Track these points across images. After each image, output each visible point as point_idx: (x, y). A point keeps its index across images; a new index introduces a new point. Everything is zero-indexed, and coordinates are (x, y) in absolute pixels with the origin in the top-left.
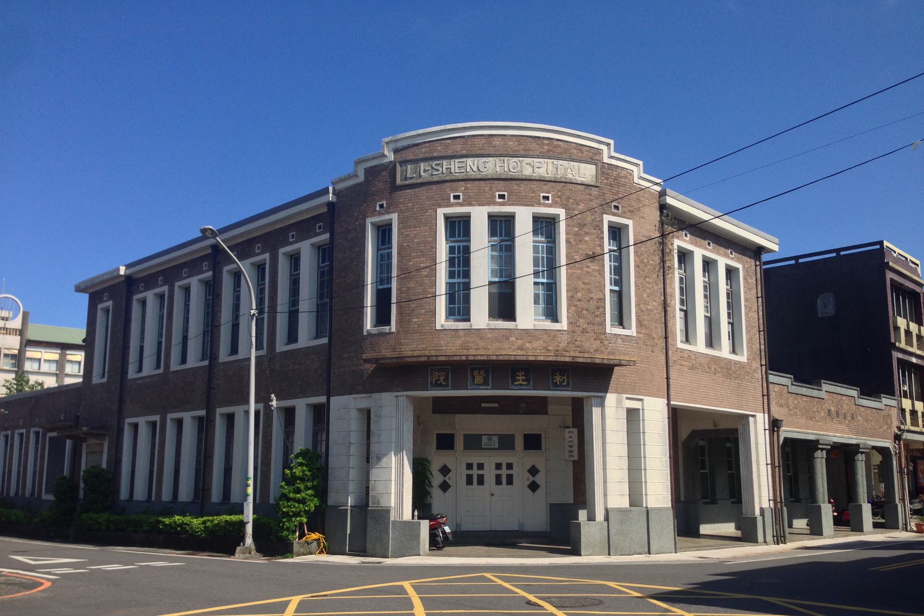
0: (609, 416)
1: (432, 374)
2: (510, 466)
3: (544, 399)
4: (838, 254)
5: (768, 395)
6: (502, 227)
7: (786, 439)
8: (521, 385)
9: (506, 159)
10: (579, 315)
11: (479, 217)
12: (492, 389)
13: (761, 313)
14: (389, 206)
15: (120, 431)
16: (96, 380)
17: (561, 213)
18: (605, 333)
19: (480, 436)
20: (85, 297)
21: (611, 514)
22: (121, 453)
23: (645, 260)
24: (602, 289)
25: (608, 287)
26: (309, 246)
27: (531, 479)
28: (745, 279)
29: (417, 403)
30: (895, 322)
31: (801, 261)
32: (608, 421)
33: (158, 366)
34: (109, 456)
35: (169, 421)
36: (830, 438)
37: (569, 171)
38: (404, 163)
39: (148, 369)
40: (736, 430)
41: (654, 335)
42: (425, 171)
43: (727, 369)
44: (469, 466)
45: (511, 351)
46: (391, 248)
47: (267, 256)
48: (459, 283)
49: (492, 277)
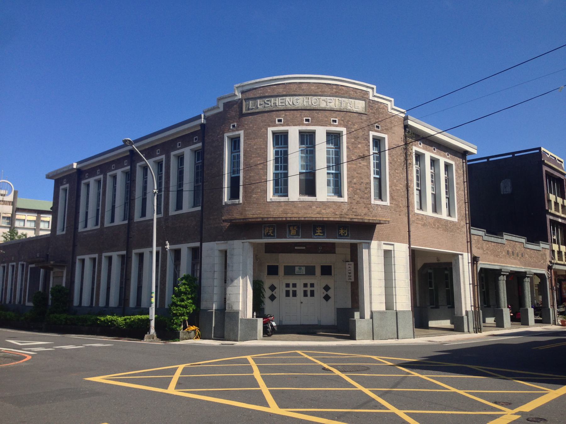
0: (373, 255)
1: (264, 229)
2: (312, 285)
3: (333, 244)
4: (513, 155)
5: (471, 242)
6: (308, 139)
7: (481, 269)
8: (319, 235)
9: (310, 97)
10: (355, 193)
11: (294, 133)
12: (301, 238)
13: (466, 192)
14: (238, 126)
15: (74, 263)
16: (59, 232)
17: (344, 130)
18: (371, 204)
19: (294, 267)
20: (52, 182)
21: (374, 315)
22: (74, 277)
23: (395, 159)
24: (369, 177)
25: (372, 176)
27: (325, 293)
28: (456, 171)
29: (256, 247)
30: (548, 197)
31: (490, 159)
32: (373, 258)
33: (97, 224)
34: (67, 279)
35: (103, 257)
36: (508, 268)
37: (349, 104)
38: (247, 99)
39: (91, 226)
40: (451, 263)
41: (401, 205)
43: (445, 226)
44: (288, 285)
45: (313, 215)
46: (239, 152)
47: (163, 157)
48: (281, 173)
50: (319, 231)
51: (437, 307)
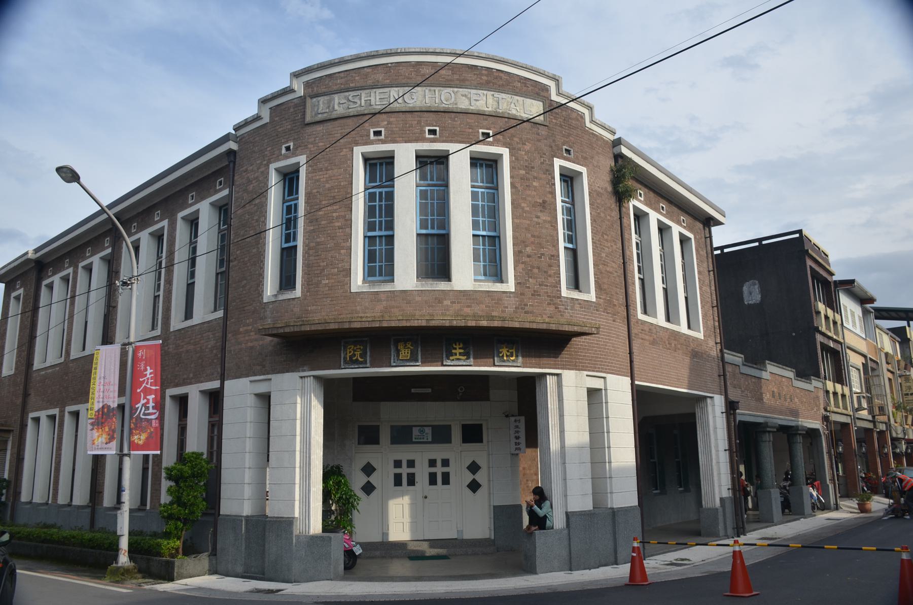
2: (446, 463)
3: (484, 378)
5: (724, 375)
6: (433, 164)
9: (437, 89)
11: (405, 156)
13: (713, 288)
14: (296, 148)
15: (23, 427)
17: (505, 152)
18: (560, 297)
19: (411, 427)
21: (572, 519)
22: (24, 450)
23: (602, 215)
25: (562, 244)
26: (208, 205)
28: (697, 250)
30: (816, 307)
31: (726, 250)
34: (12, 455)
35: (67, 414)
38: (312, 97)
40: (693, 415)
41: (616, 302)
42: (339, 104)
45: (444, 317)
46: (297, 199)
48: (380, 237)
49: (421, 228)
50: (458, 351)
51: (663, 492)
